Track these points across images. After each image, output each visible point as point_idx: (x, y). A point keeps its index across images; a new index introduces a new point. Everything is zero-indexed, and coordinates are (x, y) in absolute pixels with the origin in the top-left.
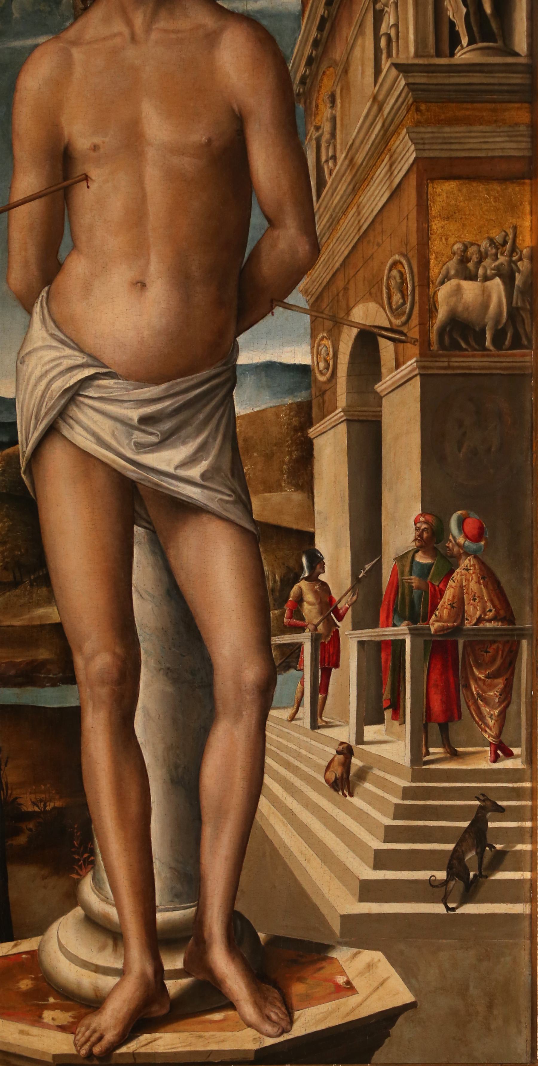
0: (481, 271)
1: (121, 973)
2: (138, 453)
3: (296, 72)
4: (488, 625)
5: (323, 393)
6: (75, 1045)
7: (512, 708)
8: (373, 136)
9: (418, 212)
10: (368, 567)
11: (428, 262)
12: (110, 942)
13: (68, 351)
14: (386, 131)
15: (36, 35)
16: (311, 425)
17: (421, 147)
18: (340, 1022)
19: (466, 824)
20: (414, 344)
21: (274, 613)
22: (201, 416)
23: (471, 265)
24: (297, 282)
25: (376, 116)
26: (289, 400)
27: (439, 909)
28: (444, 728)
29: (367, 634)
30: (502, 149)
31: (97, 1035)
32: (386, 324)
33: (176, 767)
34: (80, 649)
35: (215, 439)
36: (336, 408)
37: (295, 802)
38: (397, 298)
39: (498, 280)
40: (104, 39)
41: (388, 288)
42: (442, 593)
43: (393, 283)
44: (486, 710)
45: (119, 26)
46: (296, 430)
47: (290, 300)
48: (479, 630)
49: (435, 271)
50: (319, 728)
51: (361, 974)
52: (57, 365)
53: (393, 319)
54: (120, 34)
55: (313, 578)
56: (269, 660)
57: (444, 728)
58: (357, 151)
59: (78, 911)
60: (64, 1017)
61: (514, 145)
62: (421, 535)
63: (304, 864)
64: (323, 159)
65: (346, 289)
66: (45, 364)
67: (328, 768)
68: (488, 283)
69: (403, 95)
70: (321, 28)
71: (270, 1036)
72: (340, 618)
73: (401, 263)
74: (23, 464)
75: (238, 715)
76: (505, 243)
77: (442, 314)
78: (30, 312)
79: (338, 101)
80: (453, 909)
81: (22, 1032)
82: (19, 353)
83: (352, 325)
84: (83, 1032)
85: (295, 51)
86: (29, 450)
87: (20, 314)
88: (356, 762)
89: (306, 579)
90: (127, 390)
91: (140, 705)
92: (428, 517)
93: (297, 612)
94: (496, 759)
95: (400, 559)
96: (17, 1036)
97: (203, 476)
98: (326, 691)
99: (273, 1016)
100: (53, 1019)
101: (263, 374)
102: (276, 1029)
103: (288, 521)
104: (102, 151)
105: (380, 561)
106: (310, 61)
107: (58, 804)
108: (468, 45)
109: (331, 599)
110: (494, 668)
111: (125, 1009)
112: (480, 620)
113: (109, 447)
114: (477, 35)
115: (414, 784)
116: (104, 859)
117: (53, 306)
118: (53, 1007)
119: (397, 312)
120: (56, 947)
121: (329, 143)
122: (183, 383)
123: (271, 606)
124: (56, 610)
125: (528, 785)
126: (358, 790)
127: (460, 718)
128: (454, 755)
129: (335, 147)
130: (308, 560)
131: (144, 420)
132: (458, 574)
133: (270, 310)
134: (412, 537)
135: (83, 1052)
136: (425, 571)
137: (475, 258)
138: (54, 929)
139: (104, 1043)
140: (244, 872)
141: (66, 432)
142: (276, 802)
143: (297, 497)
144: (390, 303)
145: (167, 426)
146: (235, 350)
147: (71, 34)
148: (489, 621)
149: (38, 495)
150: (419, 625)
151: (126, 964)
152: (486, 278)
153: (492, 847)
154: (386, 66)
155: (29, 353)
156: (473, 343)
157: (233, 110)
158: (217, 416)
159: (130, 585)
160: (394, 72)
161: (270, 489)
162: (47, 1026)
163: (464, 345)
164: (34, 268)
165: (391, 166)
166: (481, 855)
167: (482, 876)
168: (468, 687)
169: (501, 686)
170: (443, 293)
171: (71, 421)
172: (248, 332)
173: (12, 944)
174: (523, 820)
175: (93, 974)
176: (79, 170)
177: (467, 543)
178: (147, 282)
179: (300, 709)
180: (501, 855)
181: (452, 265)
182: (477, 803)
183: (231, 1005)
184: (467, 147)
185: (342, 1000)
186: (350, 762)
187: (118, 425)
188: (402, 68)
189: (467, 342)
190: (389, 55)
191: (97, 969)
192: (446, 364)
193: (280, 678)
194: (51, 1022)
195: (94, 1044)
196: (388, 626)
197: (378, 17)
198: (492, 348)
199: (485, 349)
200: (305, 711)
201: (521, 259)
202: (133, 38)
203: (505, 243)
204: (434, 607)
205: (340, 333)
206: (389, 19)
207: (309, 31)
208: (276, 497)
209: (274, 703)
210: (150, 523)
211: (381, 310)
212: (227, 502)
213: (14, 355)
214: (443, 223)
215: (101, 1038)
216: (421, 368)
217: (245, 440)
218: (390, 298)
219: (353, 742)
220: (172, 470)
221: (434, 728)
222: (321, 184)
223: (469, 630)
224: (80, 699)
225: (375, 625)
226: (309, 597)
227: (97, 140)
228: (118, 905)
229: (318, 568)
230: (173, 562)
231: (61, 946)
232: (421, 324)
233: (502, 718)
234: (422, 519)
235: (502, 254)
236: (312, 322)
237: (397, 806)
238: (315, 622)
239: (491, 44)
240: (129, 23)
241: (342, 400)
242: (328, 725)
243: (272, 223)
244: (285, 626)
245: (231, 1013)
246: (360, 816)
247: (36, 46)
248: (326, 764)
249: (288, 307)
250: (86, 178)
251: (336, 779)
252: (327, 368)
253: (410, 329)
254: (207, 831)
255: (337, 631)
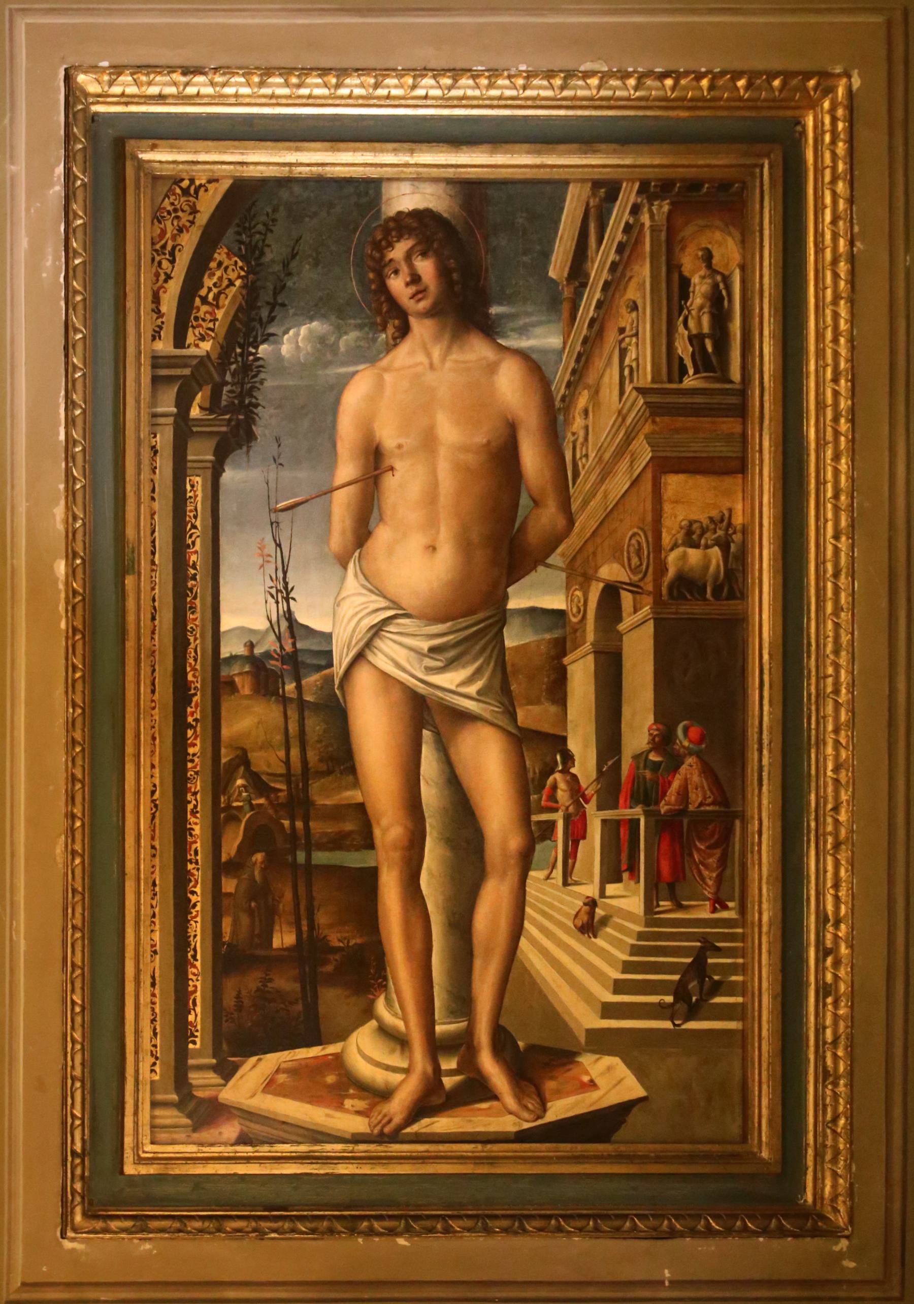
0: (703, 542)
1: (407, 1071)
2: (427, 675)
3: (558, 392)
4: (708, 808)
5: (575, 631)
6: (370, 1126)
7: (728, 872)
8: (618, 440)
9: (653, 498)
10: (610, 763)
11: (661, 535)
12: (398, 1047)
13: (374, 597)
14: (628, 437)
15: (355, 363)
16: (565, 655)
17: (655, 449)
18: (586, 1111)
19: (689, 960)
20: (648, 595)
21: (534, 797)
22: (478, 647)
23: (694, 537)
24: (556, 547)
25: (620, 426)
26: (548, 636)
27: (668, 1025)
28: (672, 887)
29: (609, 814)
30: (721, 452)
31: (386, 1119)
32: (627, 581)
33: (454, 914)
34: (378, 823)
35: (488, 664)
36: (585, 643)
37: (549, 942)
38: (635, 561)
39: (716, 549)
40: (410, 367)
41: (628, 553)
42: (670, 783)
43: (632, 549)
44: (706, 873)
45: (421, 358)
46: (553, 658)
47: (550, 561)
48: (701, 812)
49: (666, 539)
50: (569, 885)
51: (602, 1074)
52: (365, 608)
53: (632, 576)
54: (421, 363)
55: (565, 771)
56: (530, 832)
57: (672, 887)
58: (605, 451)
59: (373, 1023)
60: (361, 1105)
61: (730, 449)
62: (653, 740)
63: (556, 989)
64: (578, 456)
65: (594, 553)
66: (356, 607)
67: (576, 916)
68: (709, 551)
69: (642, 411)
70: (578, 360)
71: (527, 1121)
72: (587, 802)
73: (639, 535)
74: (337, 682)
75: (503, 875)
76: (722, 521)
77: (671, 572)
78: (345, 566)
79: (591, 414)
80: (679, 1025)
81: (328, 1115)
82: (336, 598)
83: (599, 580)
84: (376, 1117)
85: (558, 377)
86: (341, 672)
87: (338, 569)
88: (599, 912)
89: (560, 771)
90: (419, 626)
91: (425, 866)
92: (661, 727)
93: (552, 797)
94: (714, 910)
95: (636, 757)
96: (323, 1118)
97: (479, 692)
98: (575, 857)
99: (530, 1106)
100: (352, 1106)
101: (528, 616)
102: (532, 1116)
103: (546, 728)
104: (405, 449)
105: (620, 760)
106: (569, 385)
107: (359, 941)
108: (694, 374)
109: (580, 787)
110: (713, 841)
111: (410, 1099)
112: (701, 804)
113: (404, 670)
114: (700, 367)
115: (647, 929)
116: (394, 984)
117: (364, 563)
118: (352, 1097)
119: (634, 571)
120: (355, 1050)
121: (582, 445)
122: (463, 622)
123: (532, 792)
124: (360, 794)
125: (740, 930)
126: (600, 933)
127: (684, 877)
128: (680, 907)
129: (587, 448)
130: (562, 757)
131: (432, 650)
132: (683, 769)
133: (534, 568)
134: (646, 741)
135: (376, 1131)
136: (656, 766)
137: (698, 532)
138: (354, 1035)
139: (392, 1125)
140: (507, 995)
141: (371, 657)
142: (534, 942)
143: (553, 709)
144: (630, 565)
145: (452, 653)
146: (505, 598)
147: (384, 362)
148: (709, 805)
149: (348, 698)
150: (651, 808)
151: (410, 1065)
152: (707, 547)
153: (710, 978)
154: (628, 388)
155: (344, 598)
156: (697, 596)
157: (508, 420)
158: (490, 648)
159: (418, 774)
160: (635, 393)
161: (531, 702)
162: (347, 1111)
163: (689, 597)
164: (349, 536)
165: (632, 462)
166: (701, 983)
167: (702, 1000)
168: (691, 855)
169: (718, 856)
170: (672, 558)
171: (375, 650)
172: (517, 584)
173: (320, 1048)
174: (736, 957)
175: (384, 1071)
176: (387, 462)
177: (691, 746)
178: (437, 546)
179: (554, 871)
180: (719, 984)
181: (680, 537)
182: (698, 944)
183: (495, 1097)
184: (692, 449)
185: (586, 1095)
186: (594, 912)
187: (412, 654)
188: (640, 390)
189: (692, 595)
190: (631, 381)
191: (388, 1068)
192: (674, 610)
193: (538, 847)
194: (350, 1108)
195: (384, 1126)
196: (626, 808)
197: (623, 353)
198: (711, 599)
199: (705, 599)
200: (558, 873)
201: (735, 533)
202: (432, 366)
203: (722, 521)
204: (664, 794)
205: (589, 586)
206: (632, 355)
207: (569, 363)
208: (535, 709)
209: (533, 866)
210: (435, 727)
211: (623, 570)
212: (497, 712)
213: (332, 599)
214: (672, 506)
215: (390, 1121)
216: (654, 613)
217: (513, 665)
218: (629, 559)
219: (597, 897)
220: (453, 687)
221: (663, 886)
222: (576, 475)
223: (692, 812)
224: (377, 860)
225: (615, 807)
226: (562, 785)
227: (402, 441)
228: (405, 1019)
229: (570, 763)
230: (453, 757)
231: (360, 1051)
232: (655, 580)
233: (719, 880)
234: (655, 727)
235: (720, 529)
236: (567, 578)
237: (633, 946)
238: (567, 804)
239: (711, 374)
240: (429, 355)
241: (590, 636)
242: (576, 883)
243: (536, 503)
244: (542, 808)
245: (495, 1103)
246: (601, 952)
247: (357, 372)
248: (574, 913)
249: (549, 566)
250: (392, 469)
251: (583, 924)
252: (579, 612)
253: (645, 584)
254: (478, 963)
255: (585, 812)
